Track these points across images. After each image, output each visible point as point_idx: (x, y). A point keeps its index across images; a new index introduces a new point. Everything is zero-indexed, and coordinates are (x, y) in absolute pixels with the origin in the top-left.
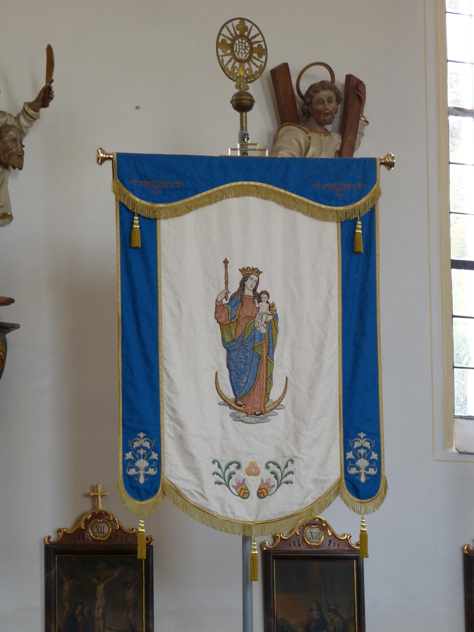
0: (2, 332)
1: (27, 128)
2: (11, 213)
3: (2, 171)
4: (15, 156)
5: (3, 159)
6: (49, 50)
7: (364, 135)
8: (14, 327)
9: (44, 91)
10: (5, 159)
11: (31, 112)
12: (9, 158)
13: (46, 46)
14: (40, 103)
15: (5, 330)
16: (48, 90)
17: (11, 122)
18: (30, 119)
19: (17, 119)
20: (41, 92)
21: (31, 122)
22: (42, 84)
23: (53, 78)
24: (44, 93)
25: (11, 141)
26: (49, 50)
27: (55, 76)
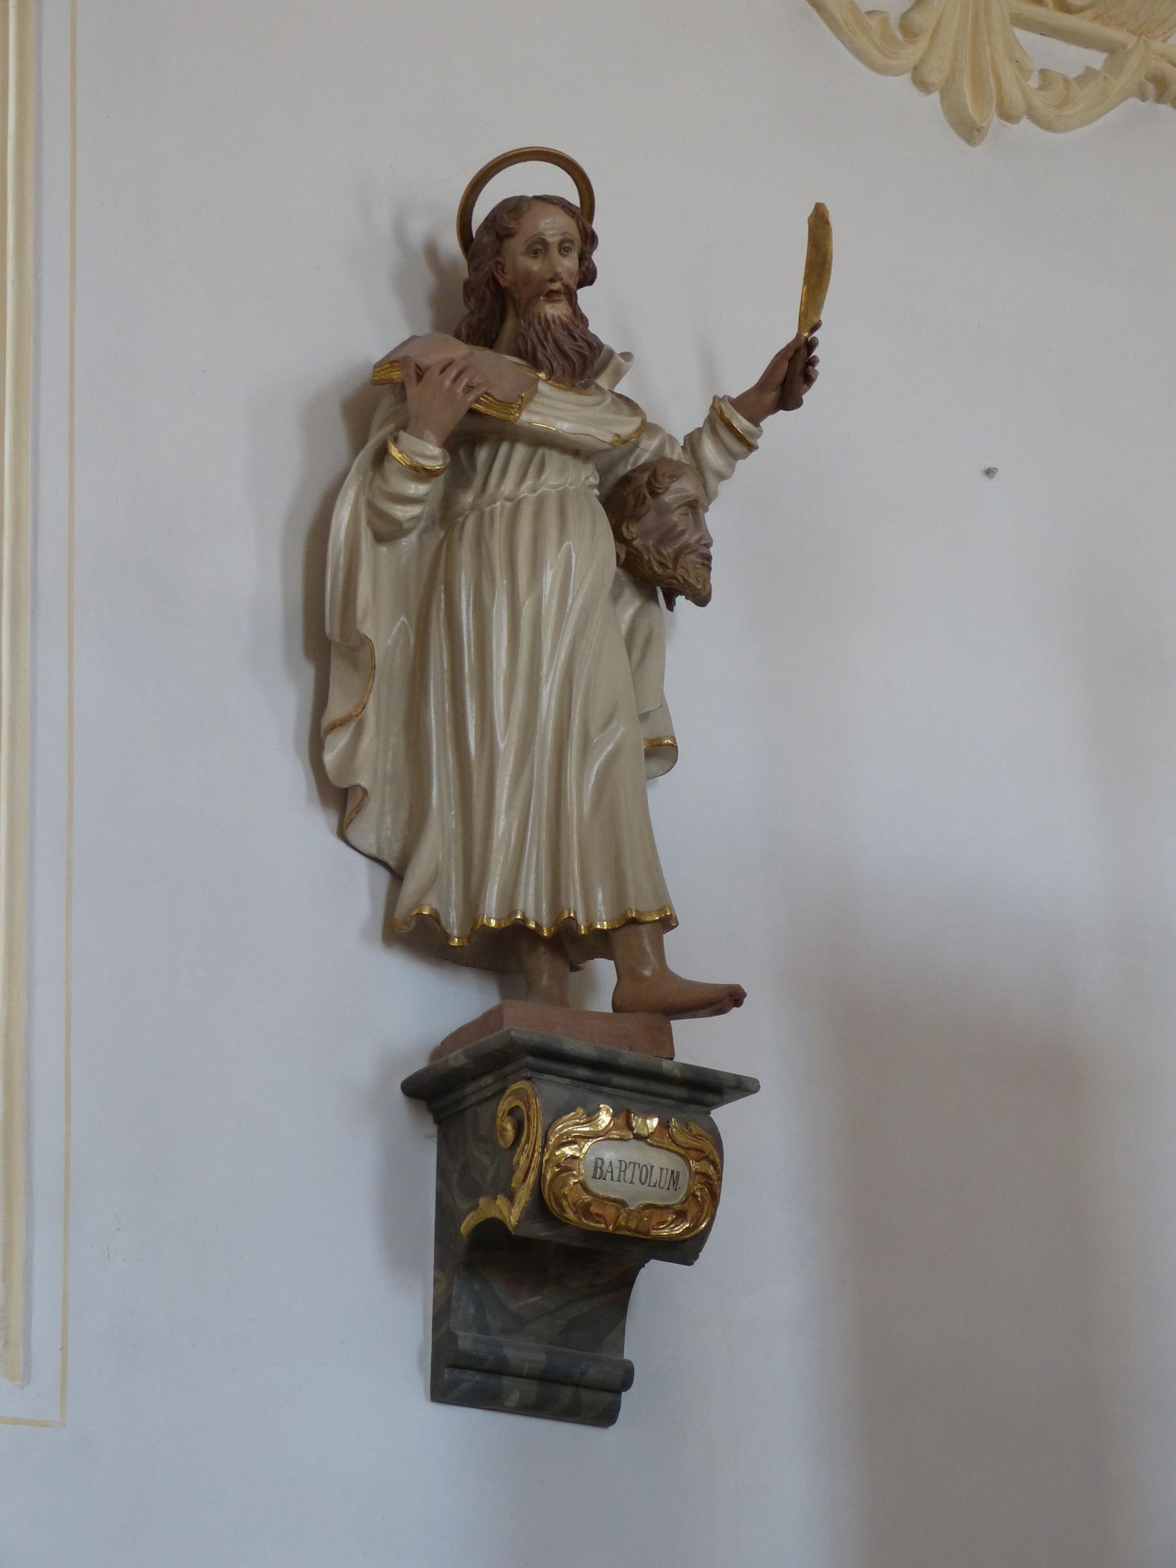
0: (700, 1103)
1: (721, 477)
2: (673, 738)
3: (640, 608)
4: (692, 557)
5: (656, 567)
6: (819, 223)
7: (441, 1392)
8: (742, 1087)
9: (791, 354)
10: (661, 564)
11: (741, 423)
12: (676, 560)
13: (810, 210)
14: (771, 396)
15: (710, 1098)
16: (804, 351)
17: (677, 454)
18: (736, 447)
19: (692, 442)
20: (780, 356)
21: (736, 457)
22: (786, 333)
23: (824, 317)
24: (791, 361)
25: (682, 510)
26: (819, 223)
27: (826, 315)
